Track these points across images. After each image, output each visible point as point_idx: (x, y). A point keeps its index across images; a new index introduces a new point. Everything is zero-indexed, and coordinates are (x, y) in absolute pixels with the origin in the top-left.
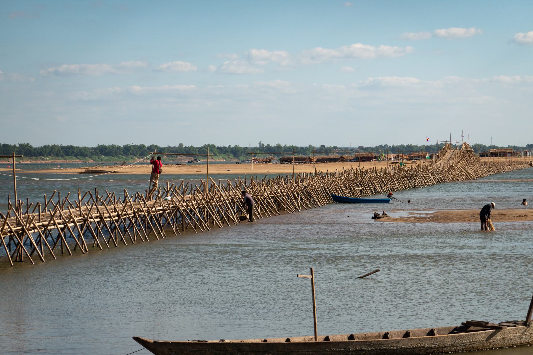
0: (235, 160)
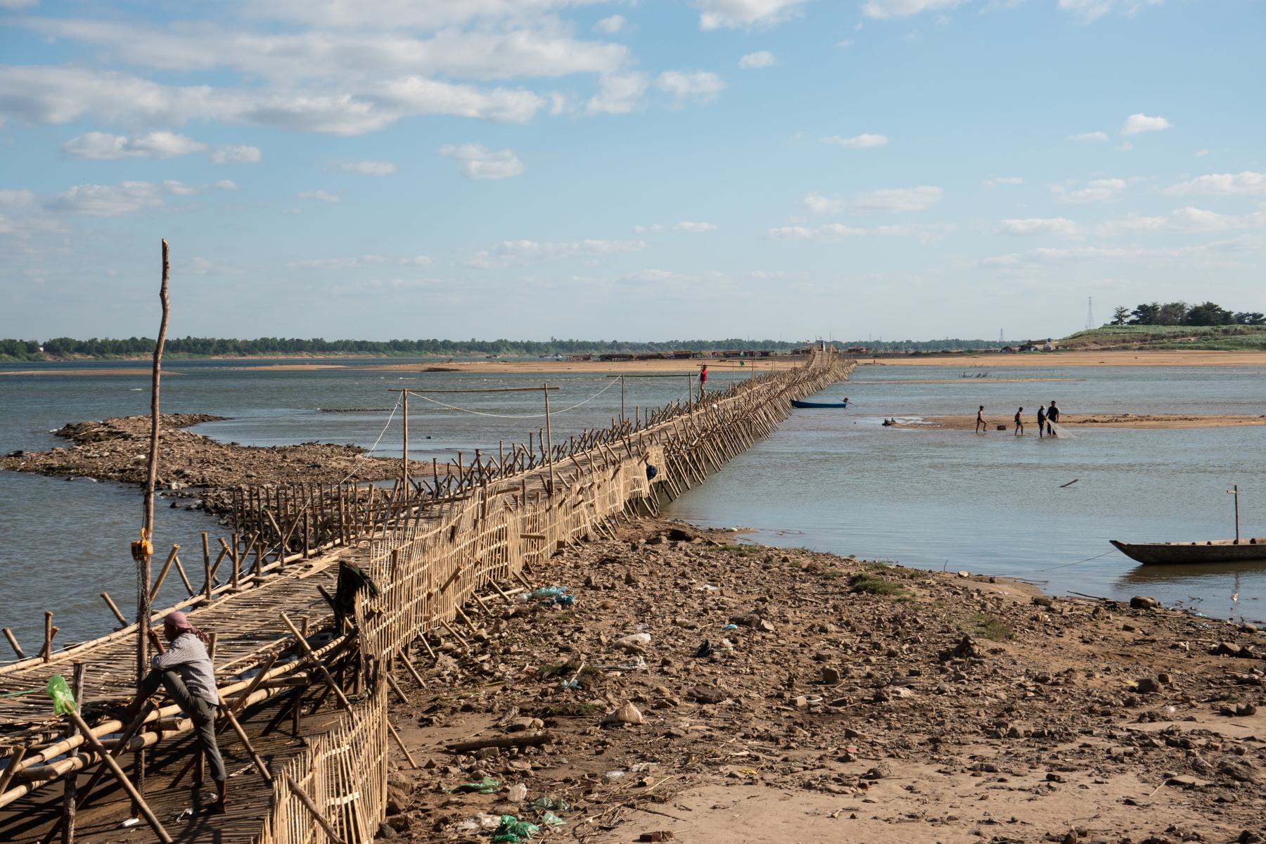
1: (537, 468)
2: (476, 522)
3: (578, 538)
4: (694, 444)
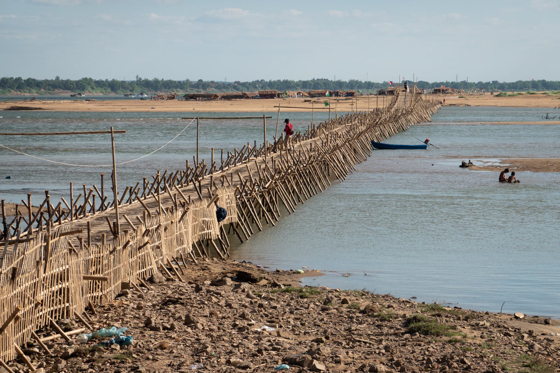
0: (113, 95)
3: (144, 279)
4: (267, 186)
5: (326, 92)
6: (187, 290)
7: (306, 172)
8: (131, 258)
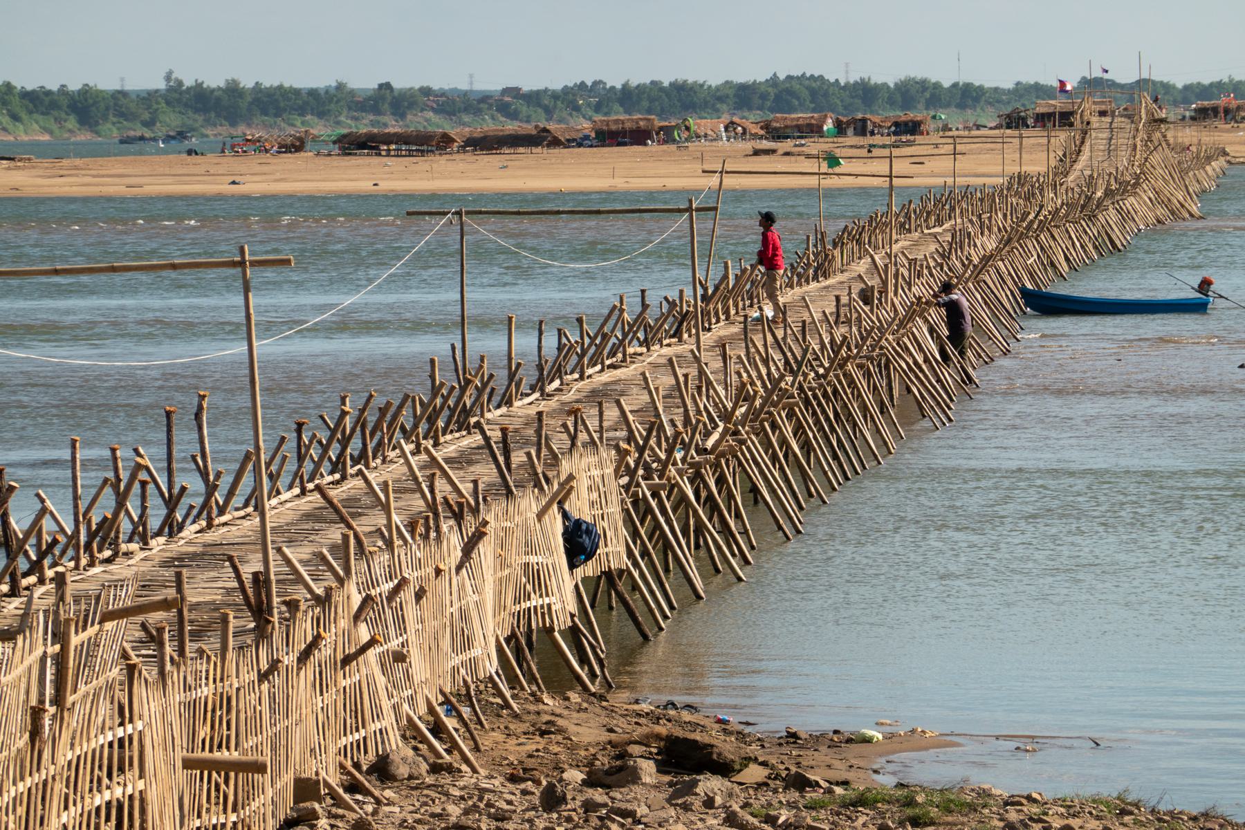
0: (84, 136)
1: (190, 531)
2: (36, 714)
3: (357, 766)
4: (710, 443)
5: (824, 122)
6: (510, 803)
7: (825, 395)
8: (322, 694)
